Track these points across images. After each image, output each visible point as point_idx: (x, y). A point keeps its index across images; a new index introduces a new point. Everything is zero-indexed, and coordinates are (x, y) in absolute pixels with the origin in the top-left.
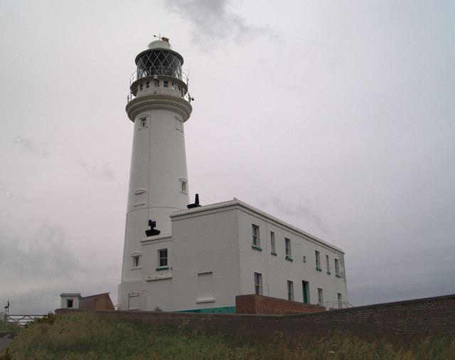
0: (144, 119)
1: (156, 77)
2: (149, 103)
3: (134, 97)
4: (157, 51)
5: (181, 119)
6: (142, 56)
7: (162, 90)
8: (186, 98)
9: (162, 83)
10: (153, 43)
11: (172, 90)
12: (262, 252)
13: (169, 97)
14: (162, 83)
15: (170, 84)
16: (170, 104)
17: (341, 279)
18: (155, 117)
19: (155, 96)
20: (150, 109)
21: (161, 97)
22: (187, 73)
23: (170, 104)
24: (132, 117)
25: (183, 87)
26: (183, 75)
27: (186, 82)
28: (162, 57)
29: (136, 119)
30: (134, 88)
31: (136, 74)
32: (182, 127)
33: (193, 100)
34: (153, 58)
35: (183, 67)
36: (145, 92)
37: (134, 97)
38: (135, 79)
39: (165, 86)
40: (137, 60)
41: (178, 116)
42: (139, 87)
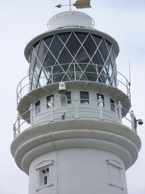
0: (45, 171)
1: (62, 86)
2: (51, 139)
3: (25, 126)
4: (63, 34)
5: (122, 166)
6: (35, 46)
7: (77, 110)
8: (126, 122)
9: (76, 96)
10: (57, 17)
11: (97, 110)
12: (35, 190)
13: (91, 125)
14: (76, 96)
15: (92, 97)
16: (92, 136)
17: (50, 167)
18: (66, 165)
19: (66, 124)
20: (56, 149)
21: (74, 124)
22: (126, 71)
23: (92, 136)
24: (24, 166)
25: (122, 101)
26: (119, 77)
27: (125, 91)
28: (90, 47)
29: (32, 169)
30: (25, 107)
31: (27, 81)
32: (123, 179)
33: (141, 123)
34: (73, 46)
35: (119, 61)
36: (47, 114)
37: (25, 126)
38: (25, 92)
39: (82, 102)
40: (28, 53)
41: (114, 159)
42: (32, 107)
